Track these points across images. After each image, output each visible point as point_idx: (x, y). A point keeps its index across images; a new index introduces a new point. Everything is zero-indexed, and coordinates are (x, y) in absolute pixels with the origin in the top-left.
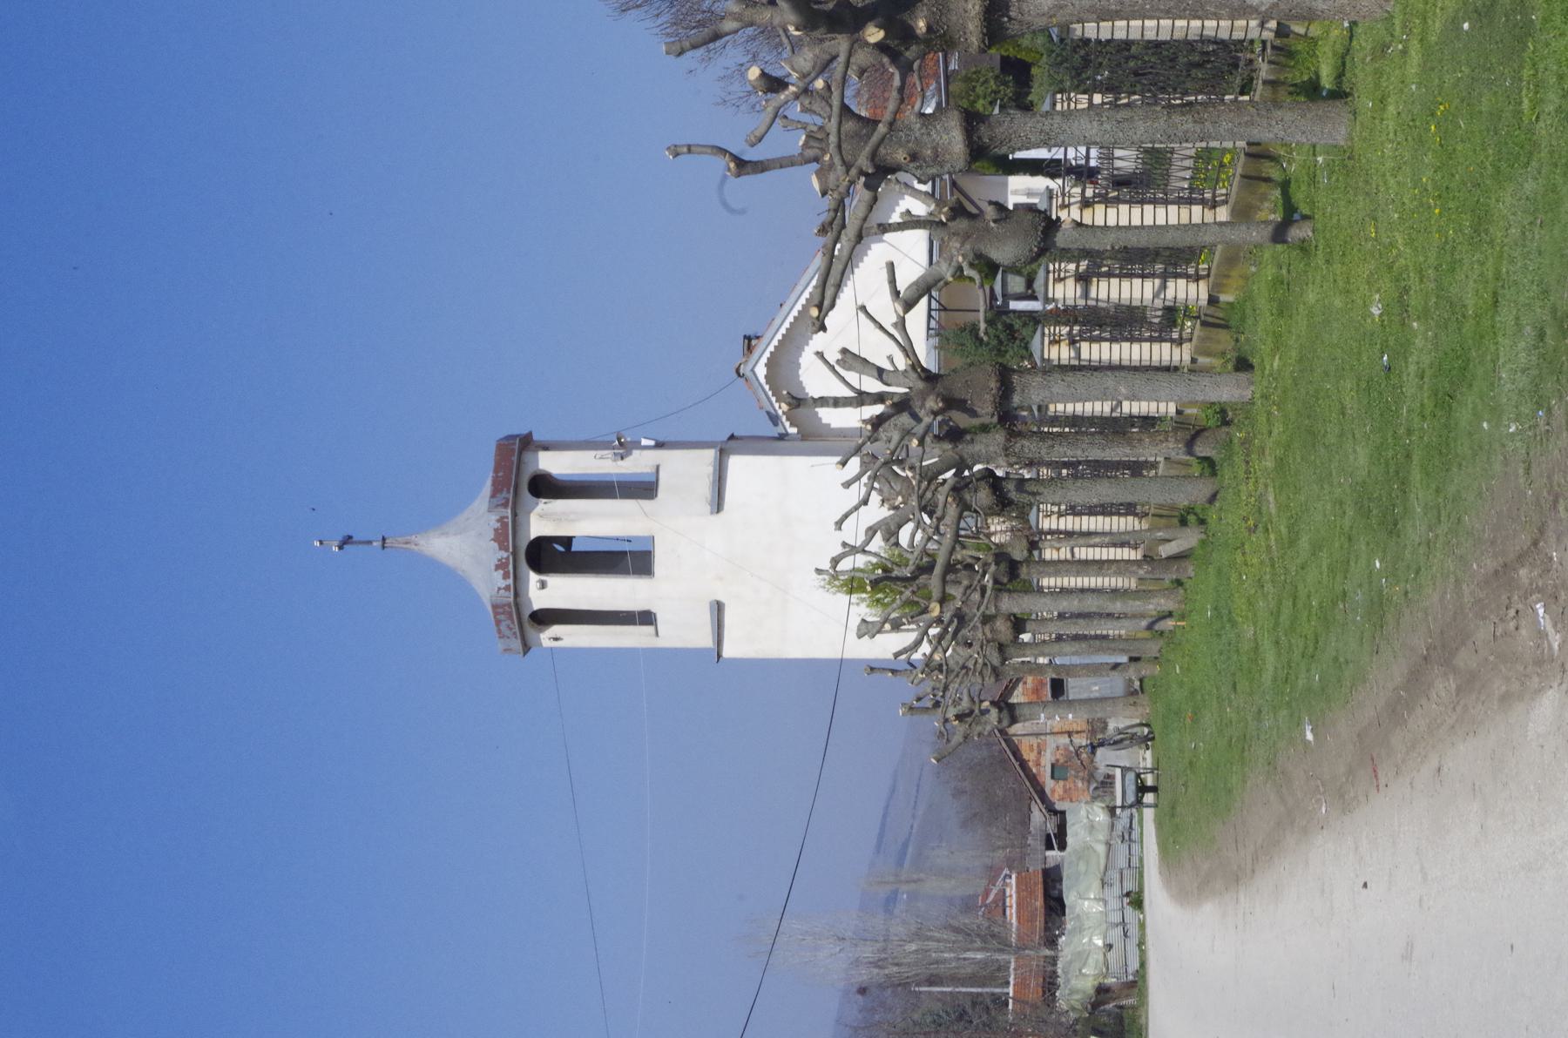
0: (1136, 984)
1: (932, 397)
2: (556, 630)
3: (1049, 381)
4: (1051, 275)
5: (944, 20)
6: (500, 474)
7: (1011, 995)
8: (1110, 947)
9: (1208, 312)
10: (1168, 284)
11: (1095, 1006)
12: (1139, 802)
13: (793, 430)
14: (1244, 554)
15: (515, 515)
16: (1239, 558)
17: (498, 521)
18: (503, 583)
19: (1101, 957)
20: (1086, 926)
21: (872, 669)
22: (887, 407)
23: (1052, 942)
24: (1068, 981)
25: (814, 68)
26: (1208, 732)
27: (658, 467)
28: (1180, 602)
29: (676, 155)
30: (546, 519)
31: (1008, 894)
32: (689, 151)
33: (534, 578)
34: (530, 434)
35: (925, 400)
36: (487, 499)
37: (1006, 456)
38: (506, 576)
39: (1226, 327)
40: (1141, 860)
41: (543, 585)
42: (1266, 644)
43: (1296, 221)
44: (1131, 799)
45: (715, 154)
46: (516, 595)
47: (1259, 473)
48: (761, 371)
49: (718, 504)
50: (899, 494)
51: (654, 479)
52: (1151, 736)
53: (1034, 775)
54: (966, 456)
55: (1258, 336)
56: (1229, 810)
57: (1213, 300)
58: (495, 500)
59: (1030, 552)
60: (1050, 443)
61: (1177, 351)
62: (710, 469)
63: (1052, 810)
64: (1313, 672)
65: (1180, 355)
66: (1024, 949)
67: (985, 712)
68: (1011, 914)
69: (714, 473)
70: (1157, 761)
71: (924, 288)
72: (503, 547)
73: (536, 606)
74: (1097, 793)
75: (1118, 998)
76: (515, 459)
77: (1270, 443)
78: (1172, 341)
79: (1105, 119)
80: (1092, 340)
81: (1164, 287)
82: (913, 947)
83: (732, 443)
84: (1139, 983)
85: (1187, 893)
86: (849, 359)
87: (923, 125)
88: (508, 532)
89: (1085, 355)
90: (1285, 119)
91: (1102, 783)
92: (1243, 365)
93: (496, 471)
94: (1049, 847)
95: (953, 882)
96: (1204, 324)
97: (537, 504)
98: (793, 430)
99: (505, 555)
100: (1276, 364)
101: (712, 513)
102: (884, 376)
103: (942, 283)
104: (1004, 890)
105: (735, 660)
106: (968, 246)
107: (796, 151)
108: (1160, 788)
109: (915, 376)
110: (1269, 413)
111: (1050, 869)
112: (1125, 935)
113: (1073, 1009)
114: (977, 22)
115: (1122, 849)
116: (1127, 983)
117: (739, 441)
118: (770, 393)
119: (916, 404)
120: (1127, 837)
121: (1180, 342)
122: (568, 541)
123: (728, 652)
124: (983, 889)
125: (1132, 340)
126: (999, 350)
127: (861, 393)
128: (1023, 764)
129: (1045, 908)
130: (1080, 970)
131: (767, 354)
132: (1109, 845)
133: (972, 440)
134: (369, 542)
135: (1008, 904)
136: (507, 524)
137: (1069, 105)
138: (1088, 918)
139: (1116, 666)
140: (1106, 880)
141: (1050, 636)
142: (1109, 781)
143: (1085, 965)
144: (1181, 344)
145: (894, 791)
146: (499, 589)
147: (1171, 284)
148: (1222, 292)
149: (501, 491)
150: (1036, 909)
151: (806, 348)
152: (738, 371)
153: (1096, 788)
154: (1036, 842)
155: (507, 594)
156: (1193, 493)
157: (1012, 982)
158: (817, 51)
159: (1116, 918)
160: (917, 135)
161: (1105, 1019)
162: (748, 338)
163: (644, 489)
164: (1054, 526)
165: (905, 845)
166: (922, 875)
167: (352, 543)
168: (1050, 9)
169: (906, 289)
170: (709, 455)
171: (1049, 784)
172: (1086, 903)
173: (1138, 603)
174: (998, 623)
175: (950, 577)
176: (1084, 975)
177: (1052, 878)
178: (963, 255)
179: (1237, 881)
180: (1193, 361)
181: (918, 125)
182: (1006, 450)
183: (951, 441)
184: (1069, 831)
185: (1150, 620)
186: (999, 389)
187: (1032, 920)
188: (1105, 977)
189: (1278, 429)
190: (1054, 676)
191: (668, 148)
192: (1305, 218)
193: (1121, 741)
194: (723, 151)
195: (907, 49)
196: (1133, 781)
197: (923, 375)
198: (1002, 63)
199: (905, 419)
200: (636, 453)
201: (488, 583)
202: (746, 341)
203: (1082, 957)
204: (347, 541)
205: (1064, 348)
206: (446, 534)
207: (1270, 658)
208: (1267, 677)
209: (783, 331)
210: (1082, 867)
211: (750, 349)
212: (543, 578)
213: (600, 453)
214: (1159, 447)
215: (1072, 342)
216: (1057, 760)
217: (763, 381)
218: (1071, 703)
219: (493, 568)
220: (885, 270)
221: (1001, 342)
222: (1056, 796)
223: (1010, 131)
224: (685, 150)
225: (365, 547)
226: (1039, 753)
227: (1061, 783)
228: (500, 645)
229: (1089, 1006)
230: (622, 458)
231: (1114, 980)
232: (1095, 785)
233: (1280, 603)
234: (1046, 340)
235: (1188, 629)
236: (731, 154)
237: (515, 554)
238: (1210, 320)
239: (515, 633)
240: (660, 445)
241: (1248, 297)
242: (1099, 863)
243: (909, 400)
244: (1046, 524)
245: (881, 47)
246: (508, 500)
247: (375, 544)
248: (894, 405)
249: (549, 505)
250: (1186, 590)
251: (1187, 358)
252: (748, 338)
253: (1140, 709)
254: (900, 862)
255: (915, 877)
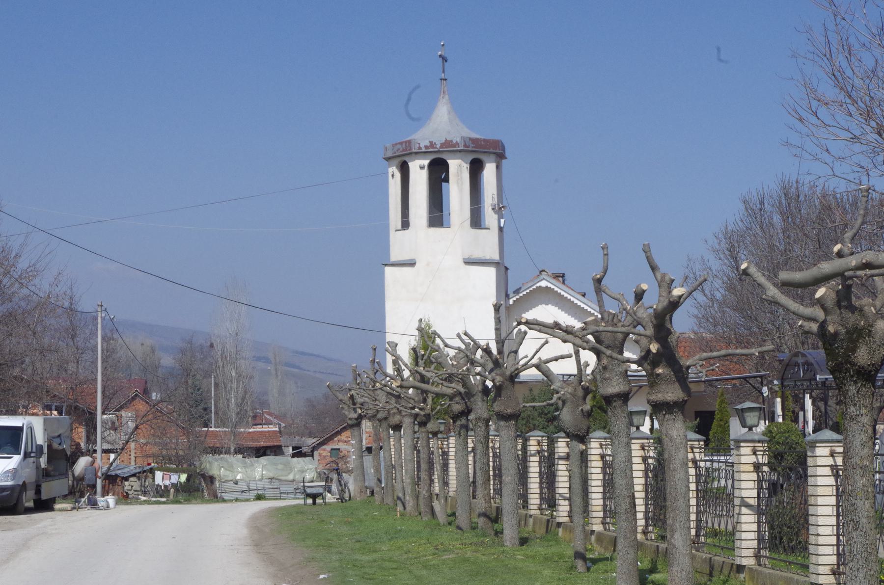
0: (215, 498)
1: (502, 379)
2: (398, 175)
3: (511, 440)
4: (646, 441)
5: (663, 382)
6: (483, 143)
7: (210, 429)
8: (236, 483)
9: (554, 523)
10: (567, 501)
11: (203, 476)
12: (309, 495)
13: (511, 302)
14: (425, 544)
15: (460, 151)
16: (423, 541)
17: (457, 142)
18: (422, 145)
19: (230, 478)
20: (247, 470)
21: (375, 349)
22: (496, 356)
23: (239, 451)
24: (217, 460)
25: (639, 318)
26: (338, 529)
27: (488, 229)
28: (411, 513)
29: (603, 248)
30: (458, 168)
31: (270, 426)
32: (605, 255)
33: (426, 162)
34: (506, 158)
35: (500, 375)
36: (469, 136)
37: (476, 418)
38: (426, 147)
39: (547, 532)
40: (285, 499)
41: (422, 168)
42: (375, 556)
43: (586, 563)
44: (309, 491)
45: (604, 267)
46: (416, 153)
47: (465, 550)
48: (543, 284)
49: (469, 262)
50: (458, 362)
51: (482, 227)
52: (344, 501)
53: (333, 439)
54: (475, 397)
55: (537, 549)
56: (293, 540)
57: (559, 525)
58: (468, 140)
59: (432, 432)
60: (483, 442)
61: (536, 507)
62: (488, 257)
63: (314, 449)
64: (355, 578)
65: (533, 509)
66: (234, 435)
67: (355, 410)
68: (256, 428)
69: (486, 260)
70: (330, 504)
71: (547, 373)
72: (442, 145)
73: (410, 164)
74: (322, 474)
75: (208, 489)
76: (491, 150)
77: (479, 555)
78: (541, 504)
79: (626, 464)
80: (540, 462)
81: (565, 499)
82: (233, 374)
83: (503, 269)
84: (215, 500)
85: (255, 524)
86: (522, 335)
87: (621, 372)
88: (450, 147)
89: (532, 459)
90: (629, 555)
91: (328, 477)
92: (523, 541)
93: (484, 140)
94: (294, 448)
95: (277, 395)
96: (548, 521)
97: (466, 163)
98: (511, 302)
99: (438, 146)
100: (519, 557)
101: (464, 259)
102: (513, 354)
103: (550, 383)
104: (272, 424)
105: (384, 271)
106: (569, 396)
107: (606, 309)
108: (314, 506)
109: (513, 370)
110: (494, 554)
111: (282, 449)
112: (243, 492)
113: (201, 464)
114: (662, 398)
115: (291, 489)
116: (216, 493)
117: (504, 273)
118: (531, 289)
119: (498, 371)
120: (298, 491)
121: (540, 509)
122: (447, 180)
123: (388, 269)
124: (273, 412)
125: (541, 483)
126: (542, 413)
127: (503, 343)
128: (339, 433)
129: (259, 447)
130: (222, 467)
131: (553, 287)
132: (293, 481)
133: (484, 401)
134: (444, 72)
135: (264, 426)
136: (455, 147)
137: (647, 446)
138: (252, 471)
139: (380, 481)
140: (274, 480)
141: (432, 447)
142: (329, 481)
143: (226, 469)
144: (539, 509)
145: (328, 360)
146: (419, 144)
147: (567, 502)
148: (563, 529)
149: (473, 143)
150: (259, 442)
151: (557, 308)
152: (543, 271)
153: (325, 474)
154: (297, 441)
155: (417, 148)
156: (462, 519)
157: (217, 429)
158: (647, 319)
159: (252, 486)
160: (616, 370)
161: (197, 482)
162: (563, 276)
163: (476, 221)
164: (634, 453)
165: (299, 368)
166: (280, 377)
167: (443, 62)
168: (670, 434)
169: (548, 367)
170: (496, 257)
171: (328, 447)
172: (260, 469)
173: (409, 491)
174: (398, 417)
175: (419, 392)
176: (220, 469)
177: (277, 450)
178: (564, 394)
179: (256, 545)
180: (531, 516)
181: (621, 370)
182: (479, 419)
183: (483, 389)
184: (300, 459)
185: (402, 498)
186: (507, 414)
187: (253, 440)
188: (219, 481)
189: (484, 558)
190: (373, 448)
191: (606, 244)
192: (588, 569)
193: (341, 485)
194: (605, 272)
195: (648, 364)
196: (318, 492)
197: (513, 374)
198: (712, 412)
199: (490, 365)
200: (496, 216)
201: (423, 137)
202: (561, 275)
203: (230, 468)
204: (444, 59)
205: (536, 448)
206: (449, 113)
207: (366, 558)
208: (358, 557)
209: (566, 295)
210: (280, 467)
211: (556, 277)
212: (426, 168)
213: (496, 197)
214: (483, 499)
215: (539, 452)
216: (341, 452)
217: (538, 285)
218: (361, 457)
219: (431, 140)
220: (568, 353)
221: (546, 414)
222: (321, 452)
223: (619, 417)
224: (605, 253)
225: (441, 70)
226: (345, 442)
227: (329, 454)
228: (388, 145)
229: (203, 472)
230: (493, 209)
231: (218, 485)
232: (326, 473)
233: (394, 561)
234: (539, 438)
235: (395, 517)
236: (604, 276)
237: (439, 152)
238: (550, 524)
239: (395, 153)
240: (501, 229)
241: (557, 541)
242: (282, 476)
243: (500, 367)
244: (594, 448)
245: (649, 351)
246: (468, 147)
247: (443, 75)
248: (497, 360)
249: (466, 170)
250: (416, 516)
251: (532, 512)
252: (563, 276)
253: (359, 495)
254: (287, 364)
255: (279, 374)
